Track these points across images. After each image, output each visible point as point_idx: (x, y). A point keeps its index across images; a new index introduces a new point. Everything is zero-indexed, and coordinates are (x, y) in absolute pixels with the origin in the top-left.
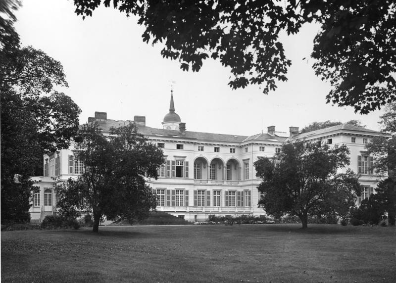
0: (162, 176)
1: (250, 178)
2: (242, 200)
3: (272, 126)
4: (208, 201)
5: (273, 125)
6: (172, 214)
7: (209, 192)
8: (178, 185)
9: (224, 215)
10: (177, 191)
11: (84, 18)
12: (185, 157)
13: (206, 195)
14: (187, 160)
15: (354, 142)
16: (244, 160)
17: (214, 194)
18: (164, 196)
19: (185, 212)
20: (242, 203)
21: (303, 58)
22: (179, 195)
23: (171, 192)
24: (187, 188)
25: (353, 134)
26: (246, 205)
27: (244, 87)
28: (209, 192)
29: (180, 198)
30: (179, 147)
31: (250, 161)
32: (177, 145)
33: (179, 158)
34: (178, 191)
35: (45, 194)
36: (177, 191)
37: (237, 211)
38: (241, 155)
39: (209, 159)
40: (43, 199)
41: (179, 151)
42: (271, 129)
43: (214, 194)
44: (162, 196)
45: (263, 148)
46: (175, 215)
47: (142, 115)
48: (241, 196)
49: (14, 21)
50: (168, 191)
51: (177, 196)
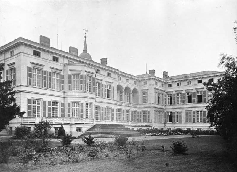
1: (149, 102)
3: (105, 58)
5: (154, 69)
6: (126, 127)
7: (82, 104)
8: (178, 109)
9: (146, 128)
10: (52, 102)
12: (43, 66)
16: (142, 90)
19: (83, 124)
20: (138, 117)
22: (55, 107)
23: (47, 103)
24: (113, 107)
25: (71, 59)
28: (82, 104)
31: (148, 91)
33: (178, 92)
34: (54, 103)
36: (53, 102)
37: (144, 125)
38: (140, 86)
42: (152, 72)
43: (86, 107)
44: (56, 108)
45: (146, 82)
46: (129, 127)
47: (39, 37)
48: (189, 118)
50: (45, 102)
51: (52, 108)
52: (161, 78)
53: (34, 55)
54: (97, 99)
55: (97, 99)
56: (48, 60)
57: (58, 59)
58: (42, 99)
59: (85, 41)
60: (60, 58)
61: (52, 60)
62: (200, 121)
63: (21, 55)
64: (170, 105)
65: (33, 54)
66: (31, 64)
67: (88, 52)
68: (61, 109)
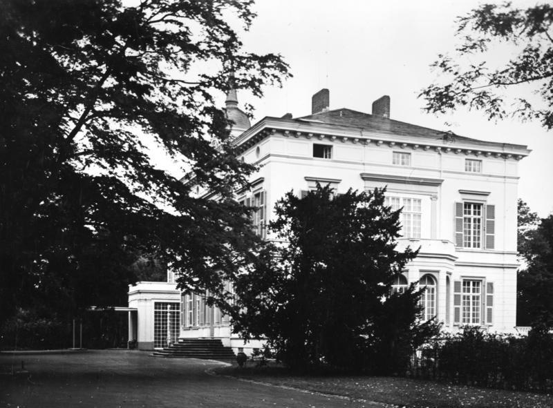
2: (464, 313)
4: (456, 309)
11: (447, 53)
12: (486, 194)
13: (482, 291)
14: (489, 201)
18: (478, 298)
21: (292, 74)
26: (199, 301)
29: (471, 301)
30: (320, 151)
32: (315, 146)
36: (466, 283)
41: (318, 161)
47: (330, 103)
52: (297, 120)
53: (315, 155)
54: (463, 257)
55: (463, 257)
56: (288, 157)
57: (330, 151)
58: (483, 279)
60: (334, 147)
61: (464, 171)
63: (270, 162)
64: (472, 248)
66: (306, 182)
68: (486, 298)
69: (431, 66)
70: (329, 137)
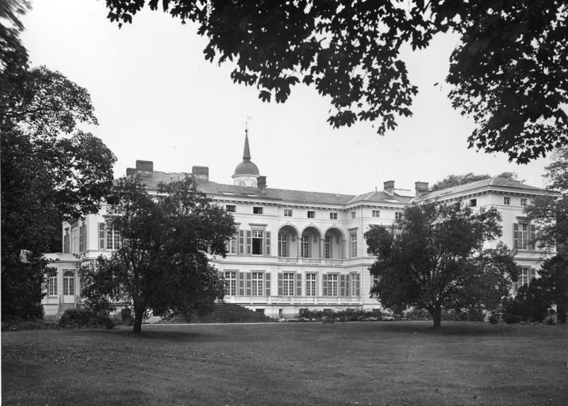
0: (232, 252)
1: (359, 256)
2: (348, 287)
5: (392, 180)
6: (246, 307)
7: (299, 276)
9: (321, 309)
10: (253, 274)
11: (120, 25)
12: (265, 225)
13: (295, 280)
14: (268, 229)
15: (508, 203)
16: (350, 230)
17: (307, 279)
18: (235, 281)
19: (265, 304)
20: (347, 291)
22: (257, 280)
23: (245, 276)
24: (268, 270)
27: (349, 125)
28: (299, 276)
29: (258, 284)
30: (257, 211)
31: (358, 231)
32: (255, 208)
34: (256, 274)
35: (64, 279)
36: (254, 274)
37: (339, 302)
38: (345, 222)
39: (300, 229)
40: (62, 286)
41: (257, 216)
42: (389, 185)
43: (307, 279)
44: (232, 281)
45: (378, 212)
46: (250, 308)
49: (19, 30)
50: (242, 275)
51: (253, 281)
59: (247, 139)
62: (232, 252)
65: (252, 212)
67: (251, 160)
69: (543, 176)
70: (313, 208)
